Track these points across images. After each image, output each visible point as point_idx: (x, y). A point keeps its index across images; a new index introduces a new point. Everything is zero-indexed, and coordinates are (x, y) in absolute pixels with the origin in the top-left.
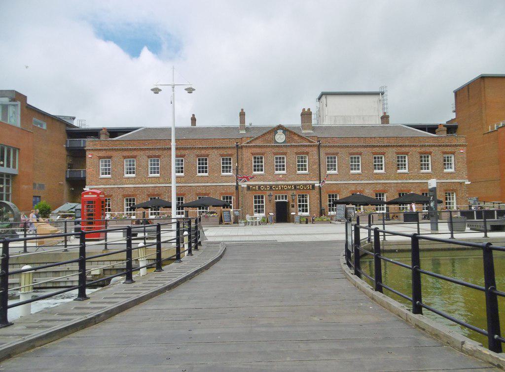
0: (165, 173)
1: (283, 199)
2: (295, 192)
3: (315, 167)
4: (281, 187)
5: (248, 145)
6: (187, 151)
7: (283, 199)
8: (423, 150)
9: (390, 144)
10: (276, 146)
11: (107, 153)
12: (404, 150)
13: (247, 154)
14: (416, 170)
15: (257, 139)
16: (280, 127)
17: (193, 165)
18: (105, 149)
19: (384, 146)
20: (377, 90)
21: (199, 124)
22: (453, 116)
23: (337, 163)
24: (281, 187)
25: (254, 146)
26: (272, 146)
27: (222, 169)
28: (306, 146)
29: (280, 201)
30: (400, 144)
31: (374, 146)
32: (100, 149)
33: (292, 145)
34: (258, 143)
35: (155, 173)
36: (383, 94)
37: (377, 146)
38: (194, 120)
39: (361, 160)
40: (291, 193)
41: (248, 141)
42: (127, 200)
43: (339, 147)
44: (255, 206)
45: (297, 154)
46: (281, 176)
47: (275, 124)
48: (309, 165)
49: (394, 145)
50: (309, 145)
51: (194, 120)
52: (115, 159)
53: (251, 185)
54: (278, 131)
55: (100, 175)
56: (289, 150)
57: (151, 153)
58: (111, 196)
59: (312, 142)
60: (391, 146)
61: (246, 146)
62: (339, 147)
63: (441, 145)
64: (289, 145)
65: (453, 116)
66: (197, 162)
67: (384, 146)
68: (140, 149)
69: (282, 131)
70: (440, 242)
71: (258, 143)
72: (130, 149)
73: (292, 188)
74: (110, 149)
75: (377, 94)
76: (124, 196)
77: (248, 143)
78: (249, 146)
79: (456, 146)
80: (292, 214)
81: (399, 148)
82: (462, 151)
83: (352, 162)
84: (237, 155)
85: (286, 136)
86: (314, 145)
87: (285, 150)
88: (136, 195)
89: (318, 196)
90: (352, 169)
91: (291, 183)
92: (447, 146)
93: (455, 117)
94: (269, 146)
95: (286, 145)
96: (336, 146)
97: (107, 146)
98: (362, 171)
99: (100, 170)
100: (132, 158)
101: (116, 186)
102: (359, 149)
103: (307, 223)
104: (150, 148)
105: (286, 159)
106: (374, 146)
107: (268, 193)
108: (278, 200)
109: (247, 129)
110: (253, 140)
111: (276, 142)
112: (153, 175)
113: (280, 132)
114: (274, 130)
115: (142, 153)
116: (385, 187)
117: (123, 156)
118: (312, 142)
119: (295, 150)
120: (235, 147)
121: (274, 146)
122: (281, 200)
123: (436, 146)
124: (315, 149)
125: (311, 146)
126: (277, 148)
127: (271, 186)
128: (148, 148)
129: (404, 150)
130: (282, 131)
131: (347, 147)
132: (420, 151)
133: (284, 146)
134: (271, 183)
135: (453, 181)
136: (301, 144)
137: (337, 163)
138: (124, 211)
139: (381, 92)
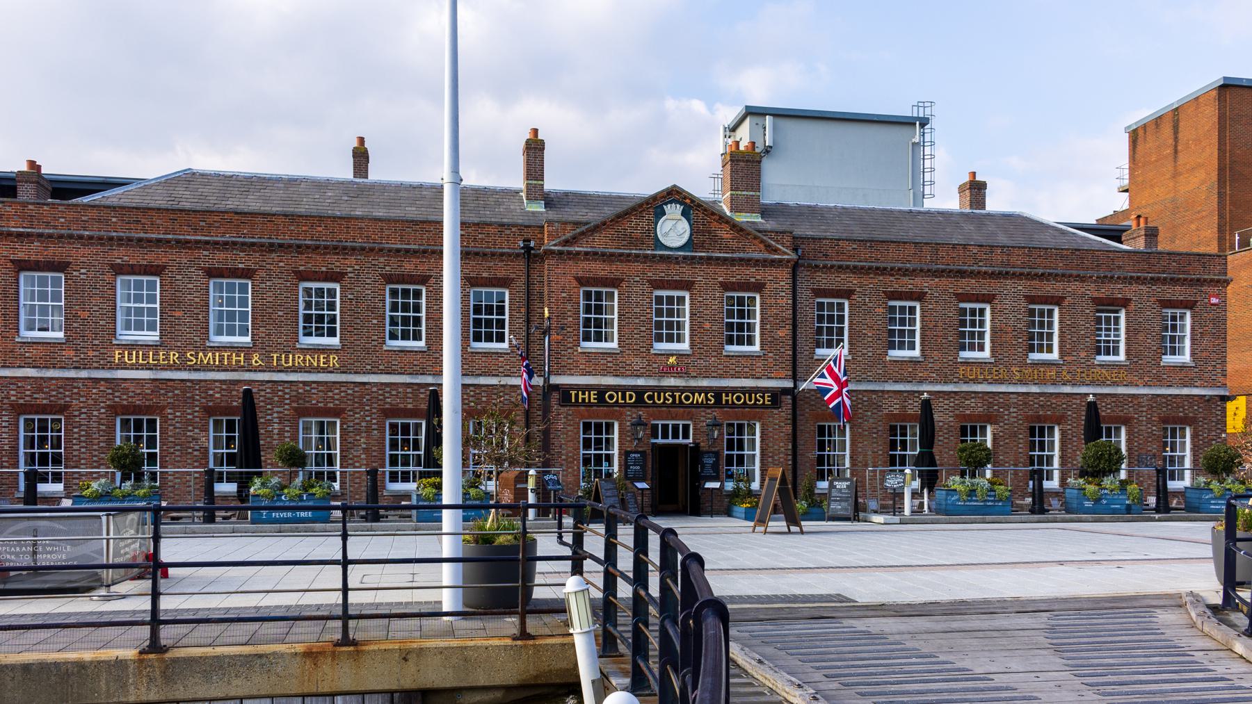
0: (269, 335)
1: (665, 436)
2: (716, 413)
3: (781, 333)
4: (673, 397)
5: (566, 248)
6: (352, 260)
7: (676, 436)
8: (1105, 291)
9: (1012, 270)
10: (661, 256)
11: (51, 250)
12: (1050, 288)
13: (558, 279)
14: (1083, 354)
15: (596, 228)
16: (674, 195)
17: (373, 309)
18: (40, 235)
19: (993, 275)
20: (906, 111)
21: (377, 173)
22: (1121, 202)
23: (507, 317)
24: (673, 397)
25: (587, 253)
26: (646, 256)
27: (301, 324)
28: (756, 263)
29: (675, 441)
30: (1040, 271)
31: (962, 274)
32: (20, 235)
33: (710, 258)
34: (599, 243)
35: (231, 332)
36: (924, 122)
37: (972, 272)
38: (361, 157)
39: (922, 317)
40: (706, 417)
41: (568, 235)
42: (125, 423)
43: (855, 270)
44: (391, 456)
45: (726, 286)
46: (672, 360)
47: (645, 186)
48: (762, 328)
49: (1021, 274)
50: (765, 260)
51: (361, 157)
52: (81, 274)
53: (573, 387)
54: (668, 208)
55: (119, 331)
56: (699, 275)
57: (219, 258)
58: (63, 409)
59: (776, 251)
60: (1014, 274)
61: (561, 253)
62: (855, 270)
63: (1159, 279)
64: (701, 258)
65: (1121, 202)
66: (388, 300)
67: (993, 275)
68: (178, 241)
69: (679, 208)
70: (68, 585)
71: (599, 243)
72: (140, 240)
73: (707, 399)
74: (61, 236)
75: (908, 123)
76: (114, 410)
77: (566, 242)
78: (569, 253)
79: (1200, 282)
80: (709, 485)
81: (1036, 282)
82: (1214, 300)
83: (659, 313)
84: (528, 284)
85: (688, 220)
86: (781, 261)
87: (686, 272)
88: (164, 408)
89: (789, 429)
90: (659, 339)
91: (705, 383)
92: (1174, 281)
93: (1126, 206)
94: (637, 256)
95: (693, 258)
96: (848, 267)
97: (48, 225)
98: (692, 345)
99: (22, 311)
100: (146, 273)
101: (84, 374)
102: (918, 280)
103: (210, 519)
104: (216, 243)
105: (692, 304)
106: (962, 274)
107: (631, 415)
108: (660, 441)
109: (551, 201)
110: (583, 233)
111: (659, 245)
112: (225, 339)
113: (673, 211)
114: (655, 205)
115: (184, 257)
116: (991, 405)
117: (112, 266)
118: (776, 251)
119: (721, 275)
120: (518, 255)
121: (654, 256)
122: (670, 441)
123: (1143, 281)
124: (784, 275)
125: (773, 263)
126: (664, 266)
127: (639, 391)
128: (207, 242)
129: (1050, 288)
130: (679, 208)
131: (882, 271)
132: (1096, 295)
133: (685, 258)
134: (641, 382)
135: (1186, 391)
136: (742, 255)
137: (507, 317)
138: (16, 465)
139: (918, 118)
